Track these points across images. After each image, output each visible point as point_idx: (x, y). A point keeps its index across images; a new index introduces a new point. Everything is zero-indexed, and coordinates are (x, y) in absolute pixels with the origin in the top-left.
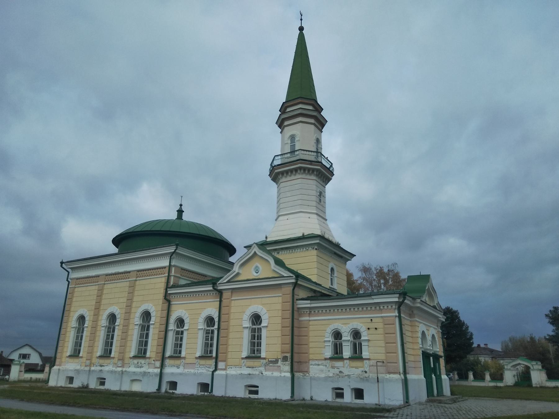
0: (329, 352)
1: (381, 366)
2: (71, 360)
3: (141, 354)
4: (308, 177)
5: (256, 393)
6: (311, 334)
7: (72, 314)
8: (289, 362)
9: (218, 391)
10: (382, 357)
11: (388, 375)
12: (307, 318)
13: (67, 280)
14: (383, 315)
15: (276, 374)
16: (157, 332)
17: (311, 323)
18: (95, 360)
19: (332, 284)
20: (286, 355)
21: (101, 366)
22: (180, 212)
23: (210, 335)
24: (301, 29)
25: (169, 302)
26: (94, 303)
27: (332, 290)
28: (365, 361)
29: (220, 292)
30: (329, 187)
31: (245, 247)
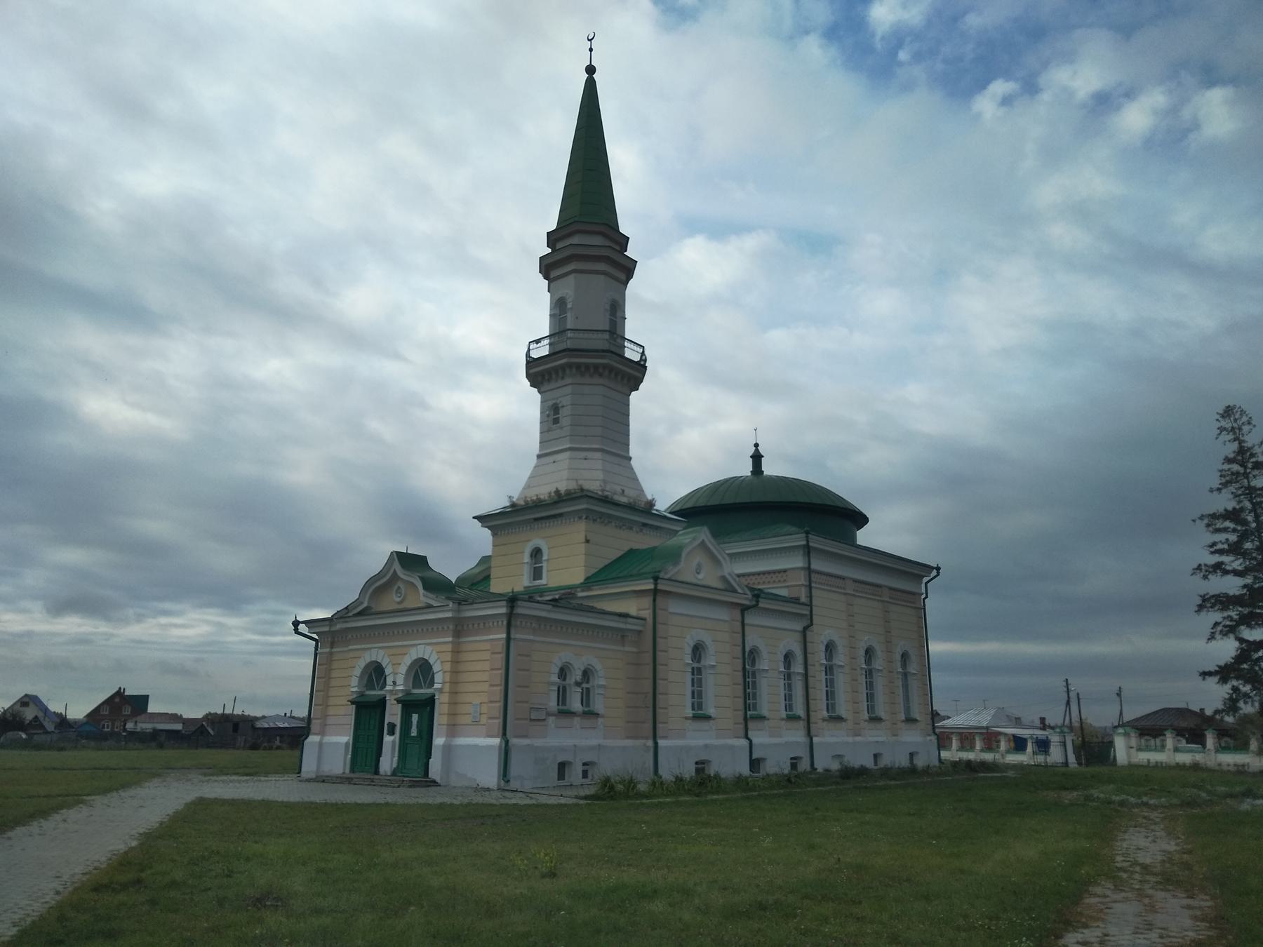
4: (561, 383)
14: (491, 637)
22: (757, 458)
24: (591, 70)
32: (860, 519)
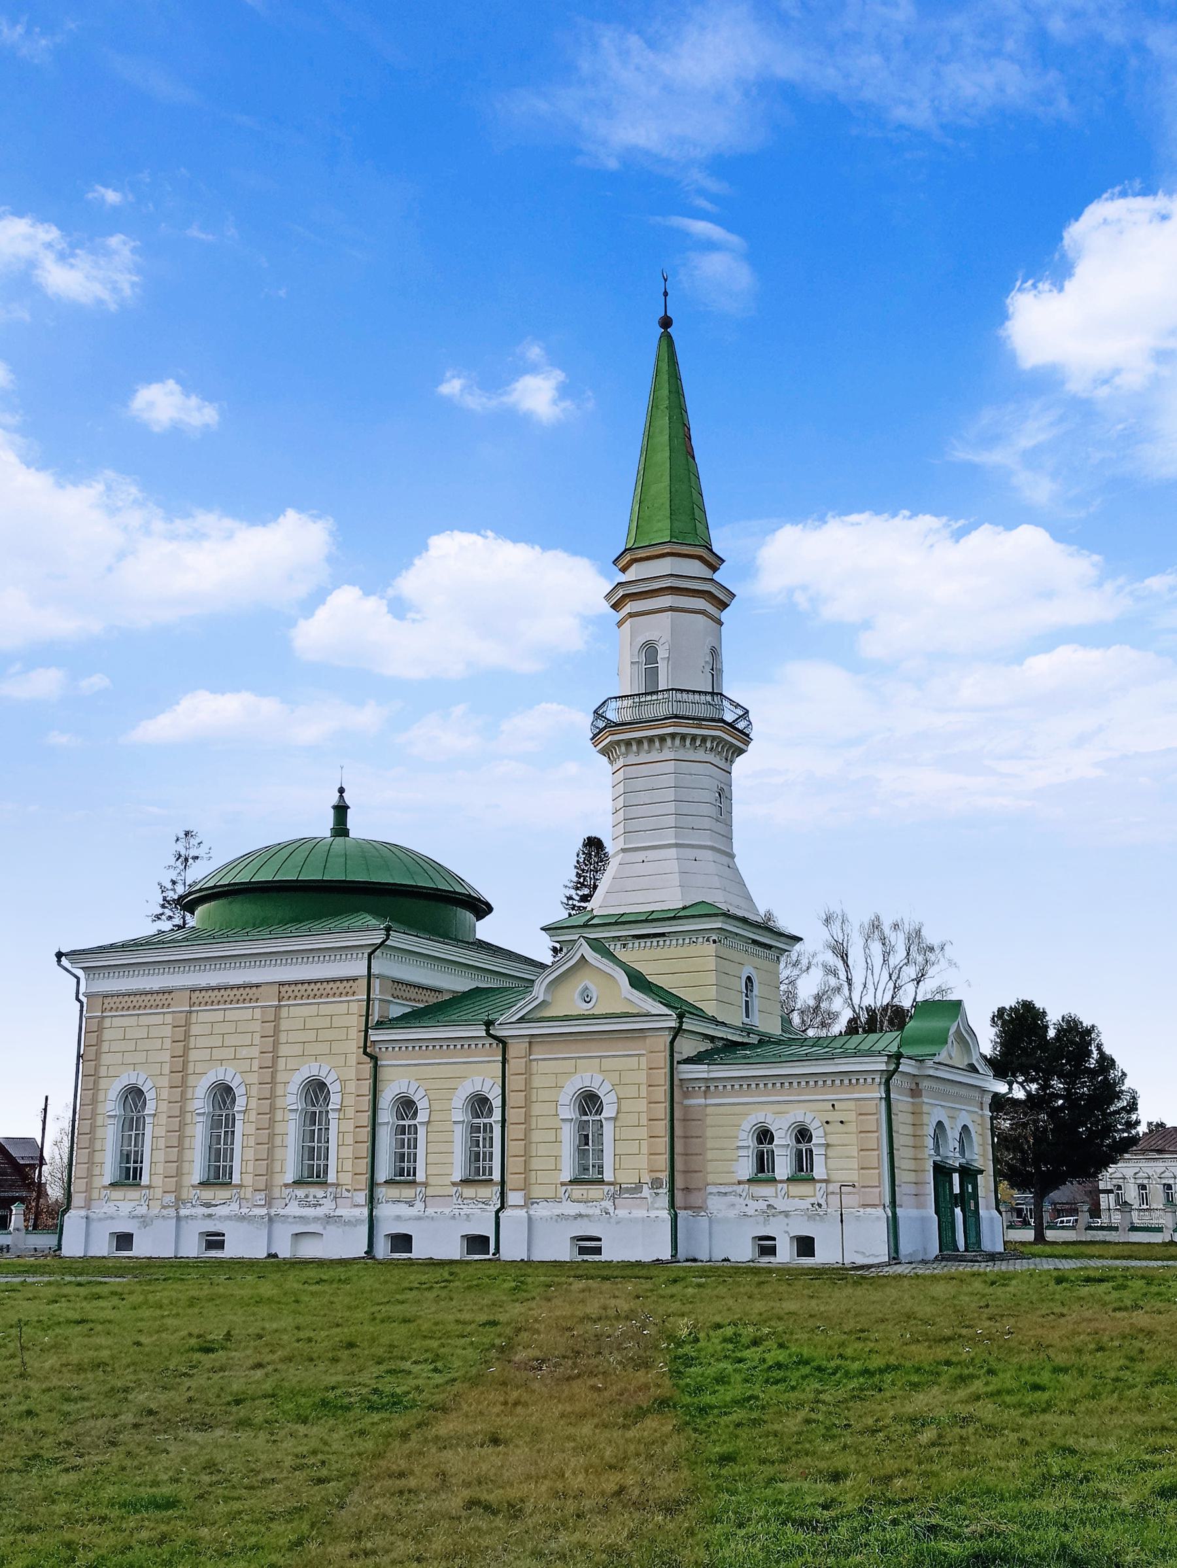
0: (746, 1168)
1: (850, 1193)
2: (118, 1194)
3: (313, 1176)
5: (598, 1250)
6: (710, 1132)
8: (664, 1190)
9: (512, 1249)
11: (861, 1210)
12: (702, 1101)
13: (78, 999)
15: (640, 1213)
17: (709, 1110)
18: (188, 1193)
19: (747, 1016)
20: (658, 1175)
21: (208, 1205)
22: (341, 810)
23: (481, 1135)
25: (374, 1059)
27: (748, 1030)
29: (502, 1042)
30: (740, 766)
31: (542, 929)
32: (481, 908)
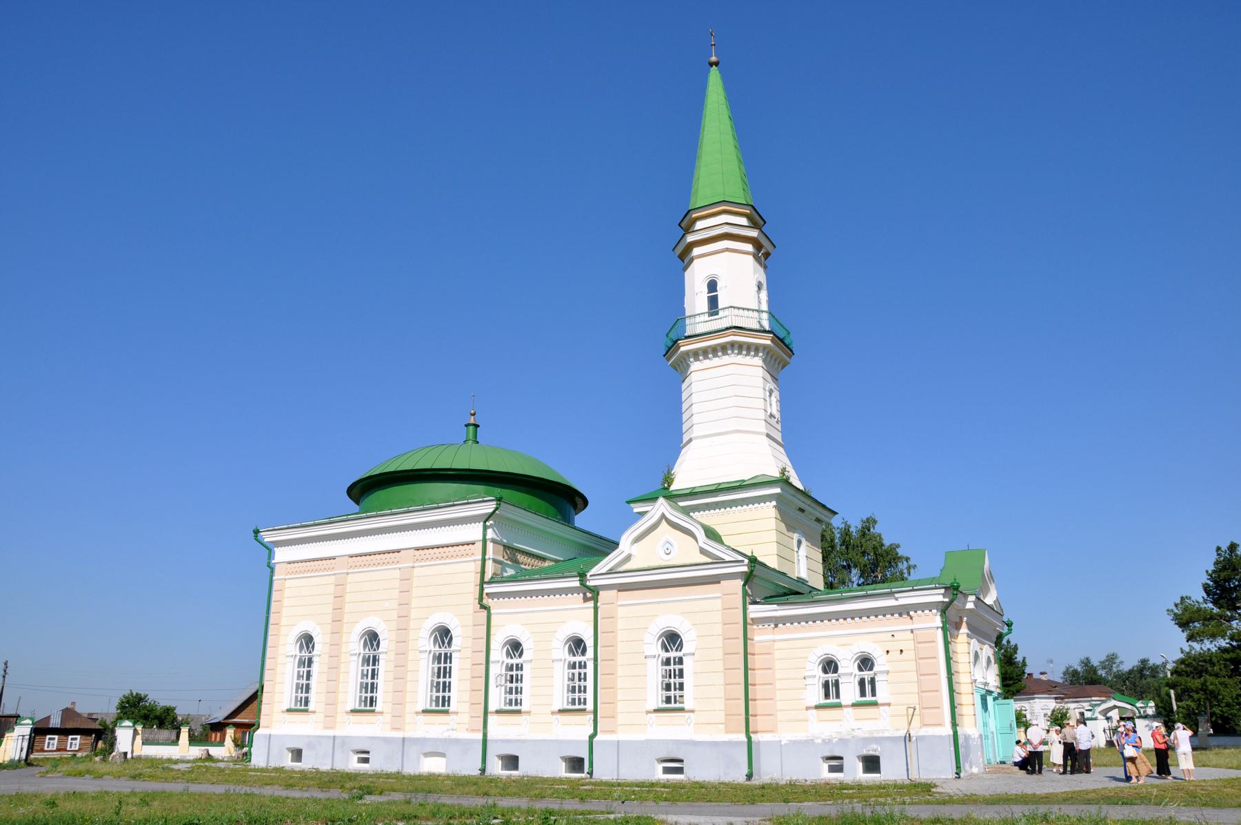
3: (441, 705)
5: (680, 771)
7: (283, 630)
9: (604, 770)
10: (914, 700)
16: (469, 666)
26: (330, 610)
28: (882, 708)
